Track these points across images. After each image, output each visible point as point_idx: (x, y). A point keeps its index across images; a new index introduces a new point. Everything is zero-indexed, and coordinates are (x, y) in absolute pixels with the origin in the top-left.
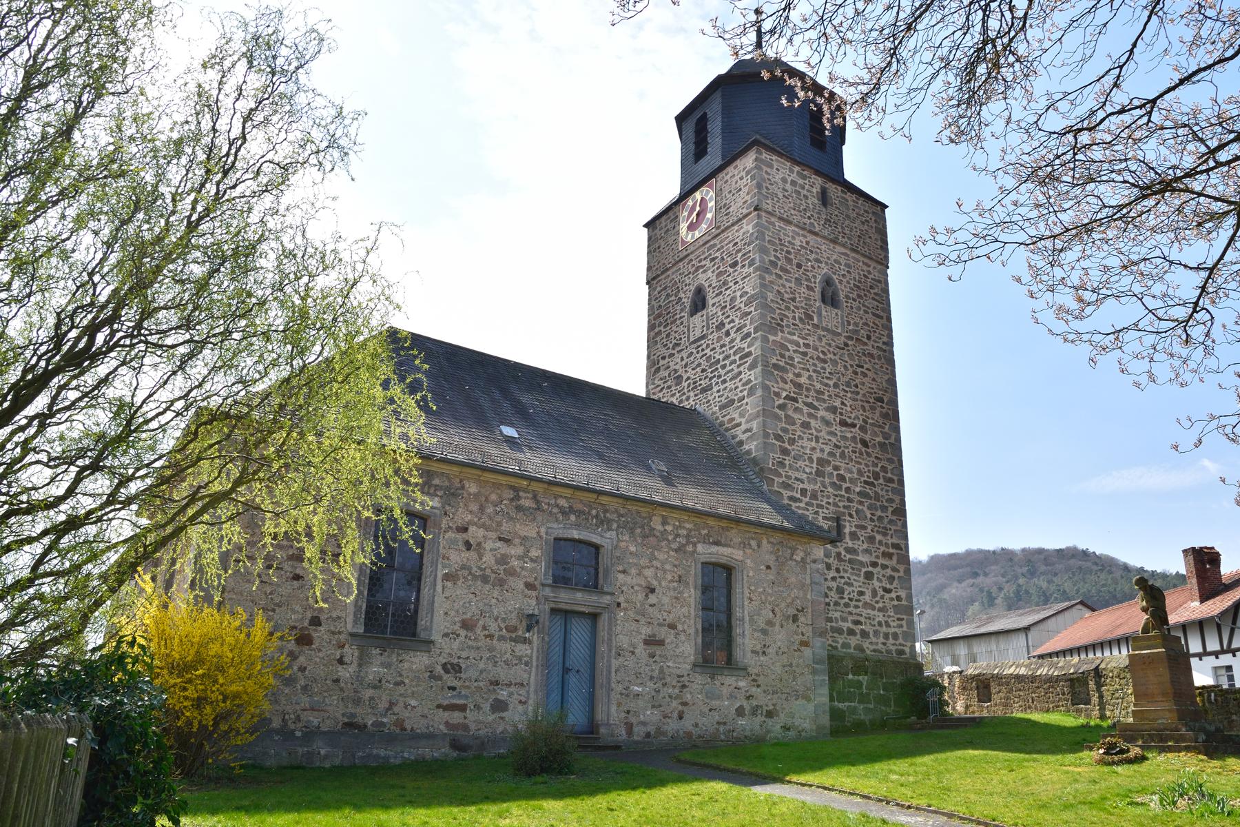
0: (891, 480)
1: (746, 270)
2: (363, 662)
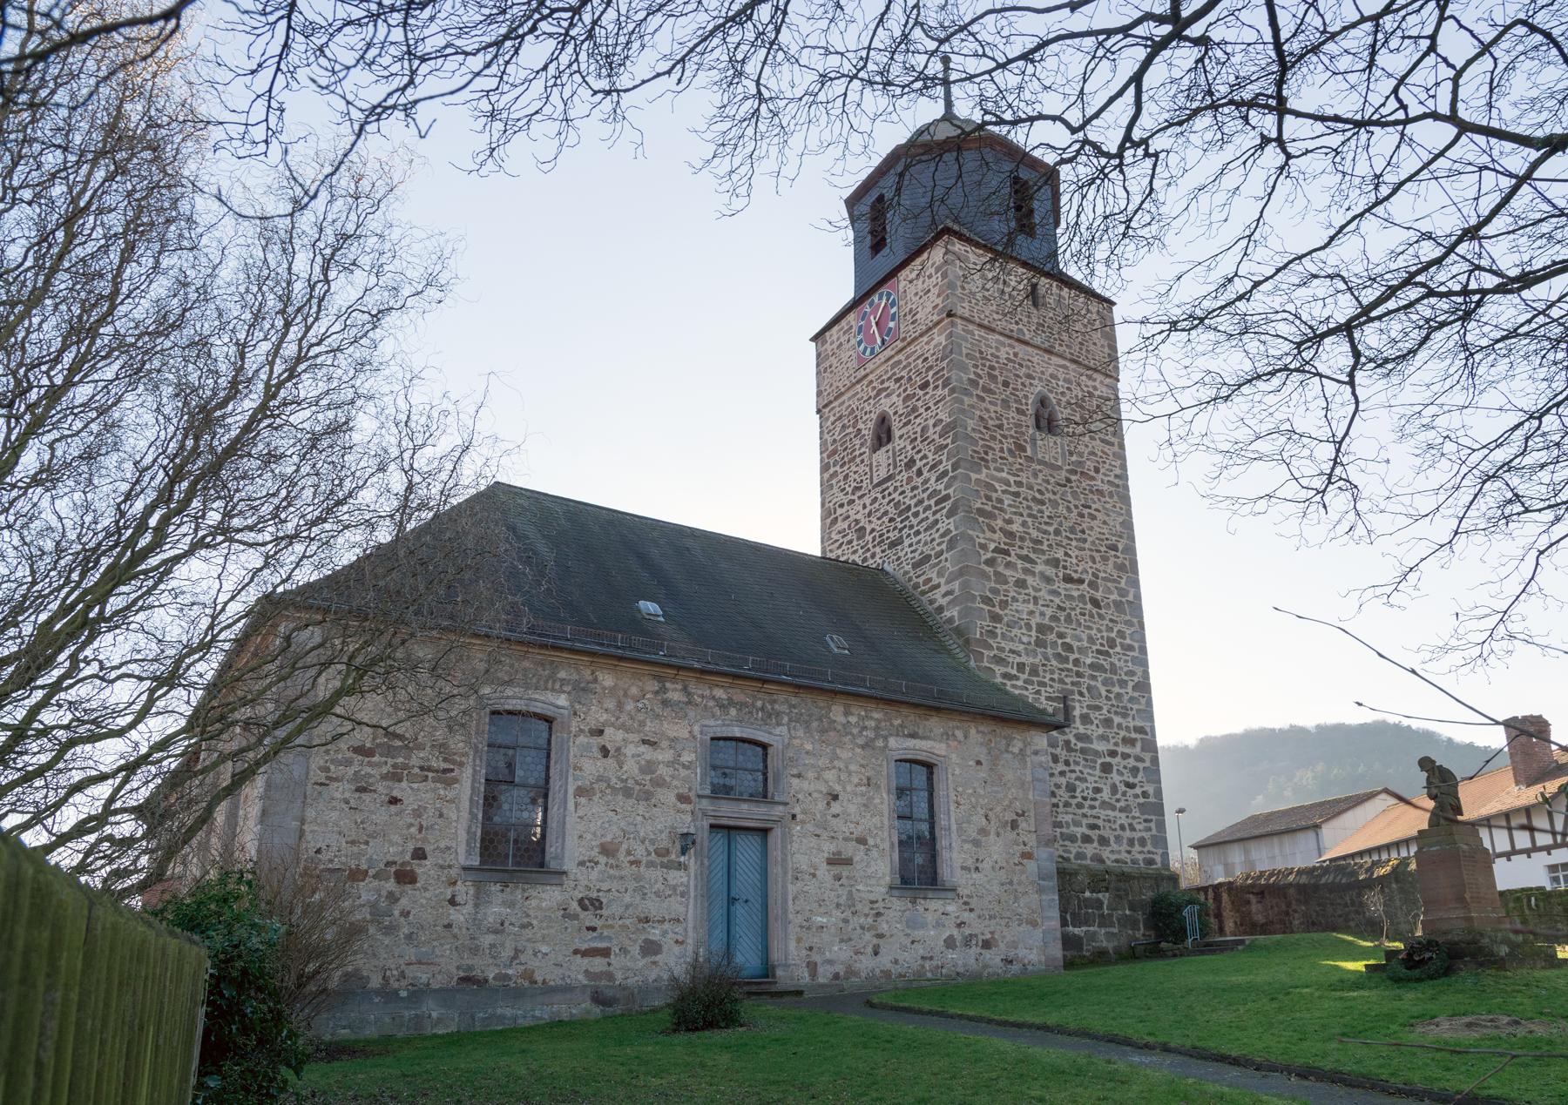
0: (1130, 648)
1: (939, 392)
2: (480, 900)
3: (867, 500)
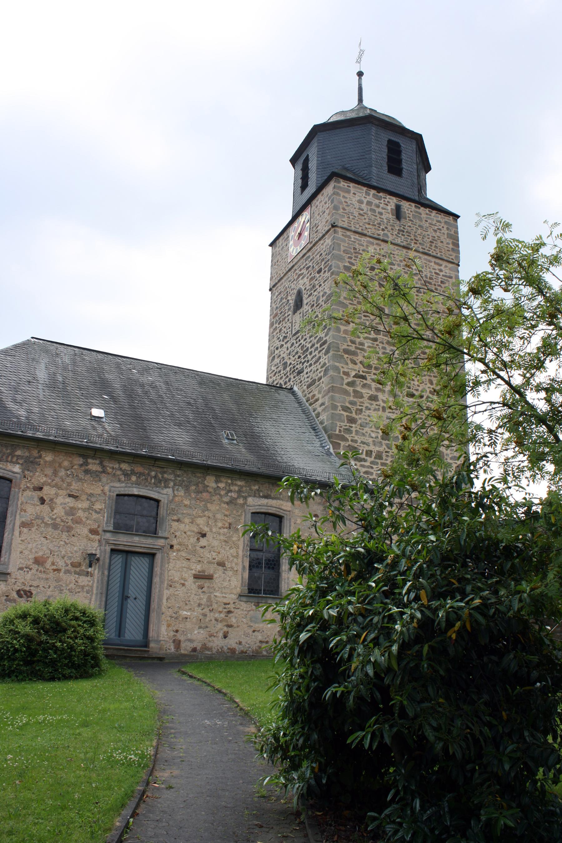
3: (289, 345)
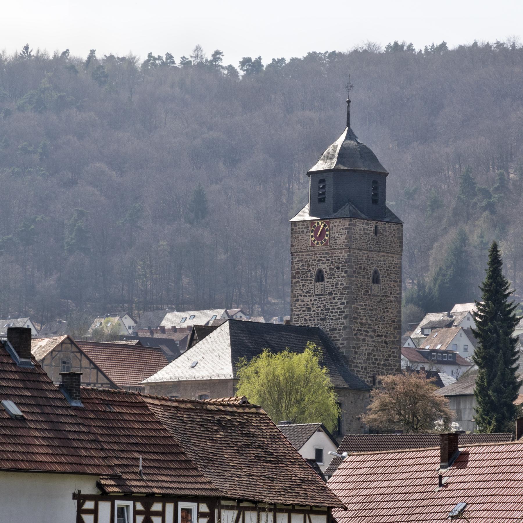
0: (396, 357)
